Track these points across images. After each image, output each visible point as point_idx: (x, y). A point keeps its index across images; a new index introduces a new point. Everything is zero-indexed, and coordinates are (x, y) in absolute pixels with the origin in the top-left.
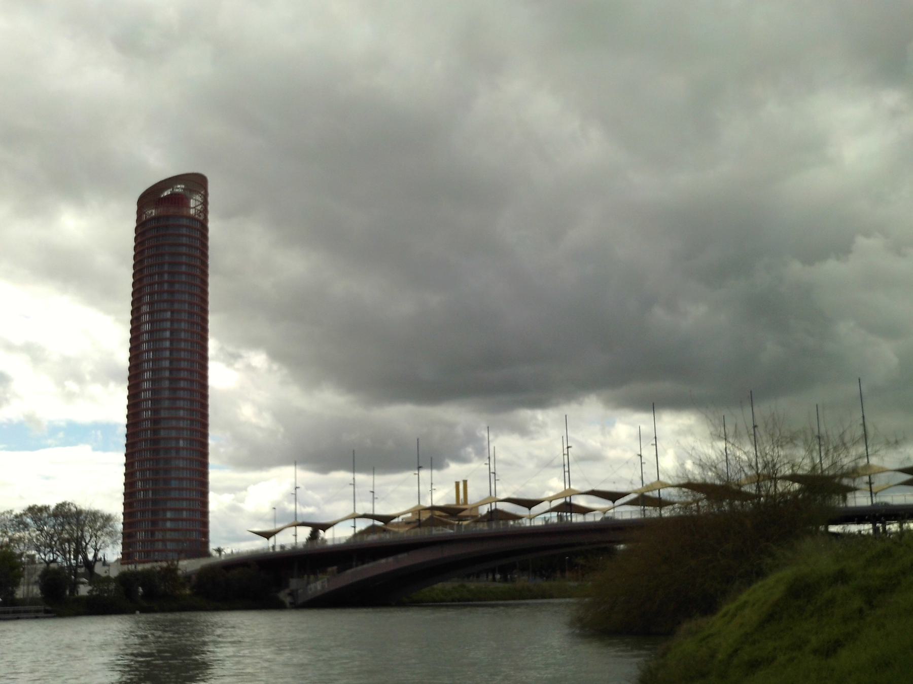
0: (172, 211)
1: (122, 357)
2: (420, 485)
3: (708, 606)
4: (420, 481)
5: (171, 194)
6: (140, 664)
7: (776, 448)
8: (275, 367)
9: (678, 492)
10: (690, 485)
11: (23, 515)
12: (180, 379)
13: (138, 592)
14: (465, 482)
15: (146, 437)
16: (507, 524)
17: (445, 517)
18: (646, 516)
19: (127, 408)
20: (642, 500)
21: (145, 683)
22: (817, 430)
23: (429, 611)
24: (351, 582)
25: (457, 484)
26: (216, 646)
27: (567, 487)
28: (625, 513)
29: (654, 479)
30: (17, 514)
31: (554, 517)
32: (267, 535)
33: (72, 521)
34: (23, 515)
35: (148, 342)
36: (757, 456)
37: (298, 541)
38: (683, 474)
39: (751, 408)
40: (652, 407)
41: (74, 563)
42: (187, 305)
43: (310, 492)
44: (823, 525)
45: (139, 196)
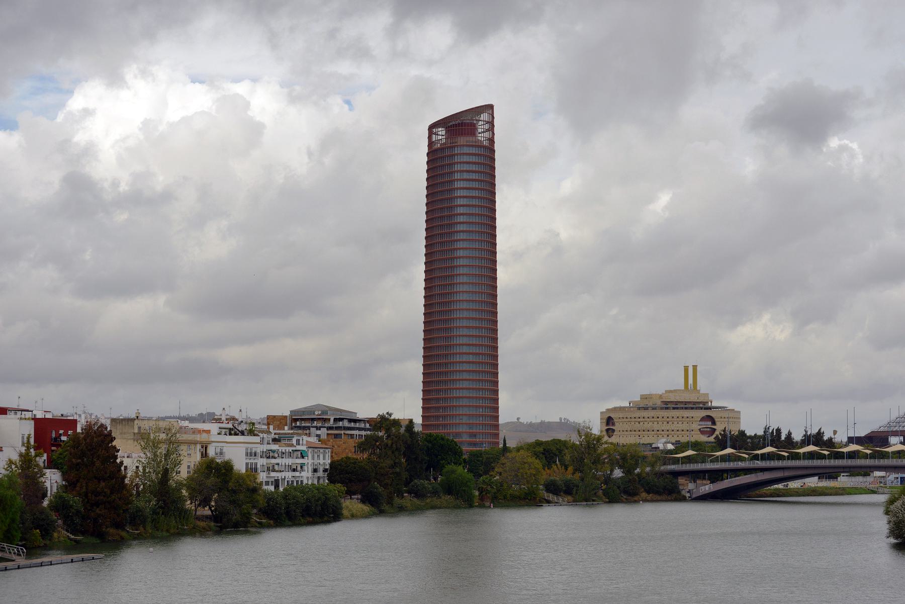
14: (695, 367)
25: (686, 369)
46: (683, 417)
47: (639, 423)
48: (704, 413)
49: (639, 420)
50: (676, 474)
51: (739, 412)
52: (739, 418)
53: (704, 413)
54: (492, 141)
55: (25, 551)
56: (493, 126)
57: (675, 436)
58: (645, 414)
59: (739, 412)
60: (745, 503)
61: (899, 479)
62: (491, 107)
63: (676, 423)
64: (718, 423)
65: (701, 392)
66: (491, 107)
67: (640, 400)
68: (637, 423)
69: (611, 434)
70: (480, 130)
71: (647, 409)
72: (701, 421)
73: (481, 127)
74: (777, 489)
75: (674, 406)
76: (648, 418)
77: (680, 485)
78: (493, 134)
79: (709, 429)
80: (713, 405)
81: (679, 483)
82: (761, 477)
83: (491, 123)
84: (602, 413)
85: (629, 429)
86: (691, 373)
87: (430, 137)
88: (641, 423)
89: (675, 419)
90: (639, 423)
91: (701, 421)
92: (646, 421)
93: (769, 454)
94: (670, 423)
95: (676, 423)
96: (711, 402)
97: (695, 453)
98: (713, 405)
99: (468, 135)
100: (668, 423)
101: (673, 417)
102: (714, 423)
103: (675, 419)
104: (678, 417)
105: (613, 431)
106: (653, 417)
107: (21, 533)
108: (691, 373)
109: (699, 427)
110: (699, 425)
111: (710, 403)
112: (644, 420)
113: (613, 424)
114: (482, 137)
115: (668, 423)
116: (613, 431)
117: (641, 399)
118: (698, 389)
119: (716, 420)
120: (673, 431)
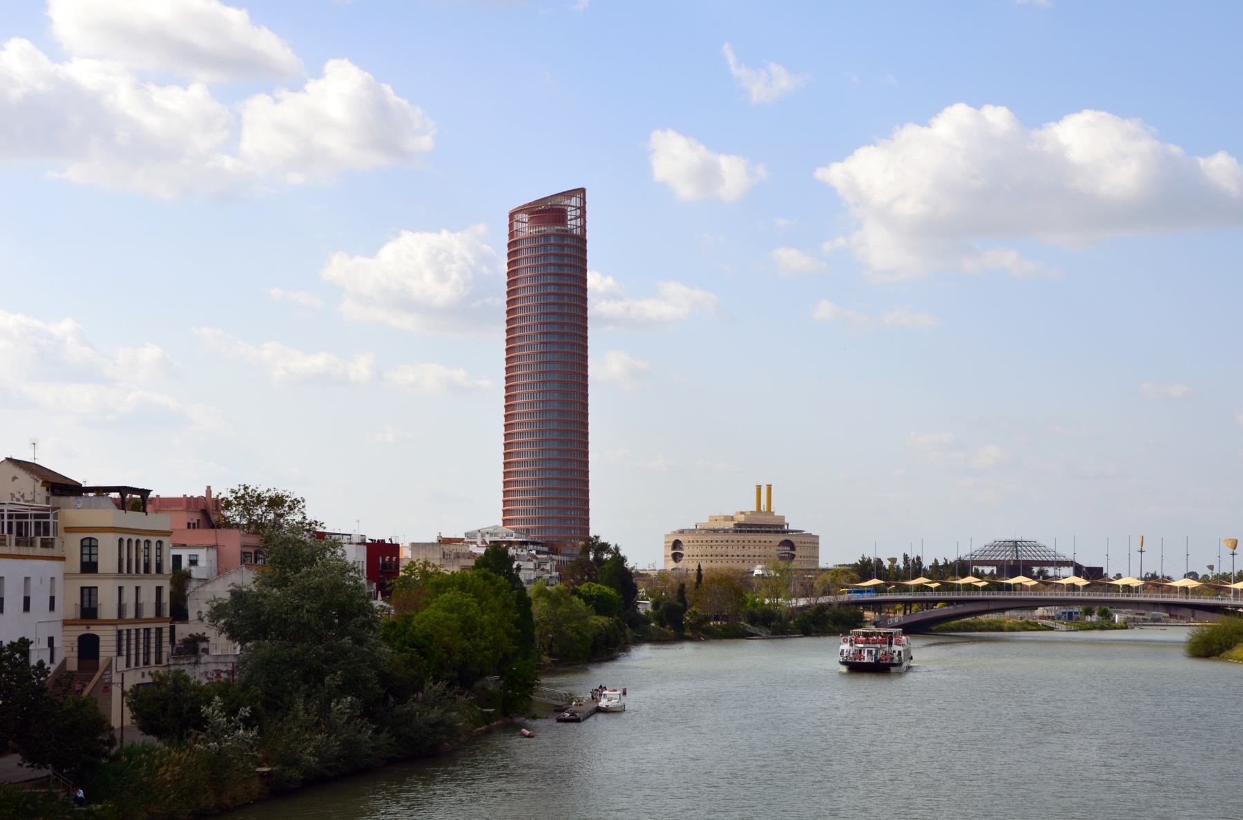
1: (457, 537)
3: (543, 546)
5: (133, 494)
6: (1086, 606)
9: (406, 558)
11: (1200, 577)
14: (769, 487)
16: (1085, 618)
17: (930, 583)
19: (965, 577)
22: (154, 599)
23: (854, 599)
24: (856, 599)
25: (759, 488)
26: (1173, 613)
28: (579, 666)
31: (440, 613)
33: (300, 704)
34: (1200, 577)
35: (266, 506)
38: (354, 563)
39: (124, 724)
42: (552, 238)
44: (197, 645)
46: (760, 542)
47: (711, 547)
48: (782, 538)
49: (711, 544)
50: (858, 603)
51: (817, 537)
52: (818, 543)
53: (782, 538)
54: (583, 227)
55: (259, 769)
56: (585, 212)
57: (724, 562)
58: (716, 537)
59: (817, 537)
60: (946, 643)
61: (1067, 615)
62: (583, 190)
63: (752, 547)
64: (797, 549)
65: (776, 514)
66: (583, 190)
67: (708, 521)
68: (709, 547)
69: (678, 559)
70: (569, 217)
71: (728, 532)
72: (779, 545)
73: (572, 213)
74: (968, 623)
75: (749, 529)
76: (722, 541)
77: (867, 621)
78: (585, 221)
79: (787, 555)
80: (790, 528)
81: (865, 616)
82: (950, 610)
83: (583, 209)
84: (667, 536)
85: (700, 554)
86: (764, 492)
87: (511, 226)
88: (714, 548)
89: (752, 543)
90: (711, 547)
91: (779, 545)
92: (719, 545)
93: (970, 584)
94: (746, 548)
95: (752, 547)
96: (788, 525)
97: (883, 582)
98: (789, 528)
99: (559, 222)
100: (744, 547)
101: (749, 542)
102: (793, 548)
103: (752, 543)
104: (755, 542)
105: (682, 555)
106: (727, 541)
107: (205, 720)
108: (764, 492)
109: (778, 552)
110: (778, 550)
111: (786, 527)
112: (717, 544)
113: (681, 549)
114: (572, 224)
115: (744, 547)
116: (682, 555)
117: (710, 520)
118: (772, 510)
119: (796, 545)
120: (749, 556)
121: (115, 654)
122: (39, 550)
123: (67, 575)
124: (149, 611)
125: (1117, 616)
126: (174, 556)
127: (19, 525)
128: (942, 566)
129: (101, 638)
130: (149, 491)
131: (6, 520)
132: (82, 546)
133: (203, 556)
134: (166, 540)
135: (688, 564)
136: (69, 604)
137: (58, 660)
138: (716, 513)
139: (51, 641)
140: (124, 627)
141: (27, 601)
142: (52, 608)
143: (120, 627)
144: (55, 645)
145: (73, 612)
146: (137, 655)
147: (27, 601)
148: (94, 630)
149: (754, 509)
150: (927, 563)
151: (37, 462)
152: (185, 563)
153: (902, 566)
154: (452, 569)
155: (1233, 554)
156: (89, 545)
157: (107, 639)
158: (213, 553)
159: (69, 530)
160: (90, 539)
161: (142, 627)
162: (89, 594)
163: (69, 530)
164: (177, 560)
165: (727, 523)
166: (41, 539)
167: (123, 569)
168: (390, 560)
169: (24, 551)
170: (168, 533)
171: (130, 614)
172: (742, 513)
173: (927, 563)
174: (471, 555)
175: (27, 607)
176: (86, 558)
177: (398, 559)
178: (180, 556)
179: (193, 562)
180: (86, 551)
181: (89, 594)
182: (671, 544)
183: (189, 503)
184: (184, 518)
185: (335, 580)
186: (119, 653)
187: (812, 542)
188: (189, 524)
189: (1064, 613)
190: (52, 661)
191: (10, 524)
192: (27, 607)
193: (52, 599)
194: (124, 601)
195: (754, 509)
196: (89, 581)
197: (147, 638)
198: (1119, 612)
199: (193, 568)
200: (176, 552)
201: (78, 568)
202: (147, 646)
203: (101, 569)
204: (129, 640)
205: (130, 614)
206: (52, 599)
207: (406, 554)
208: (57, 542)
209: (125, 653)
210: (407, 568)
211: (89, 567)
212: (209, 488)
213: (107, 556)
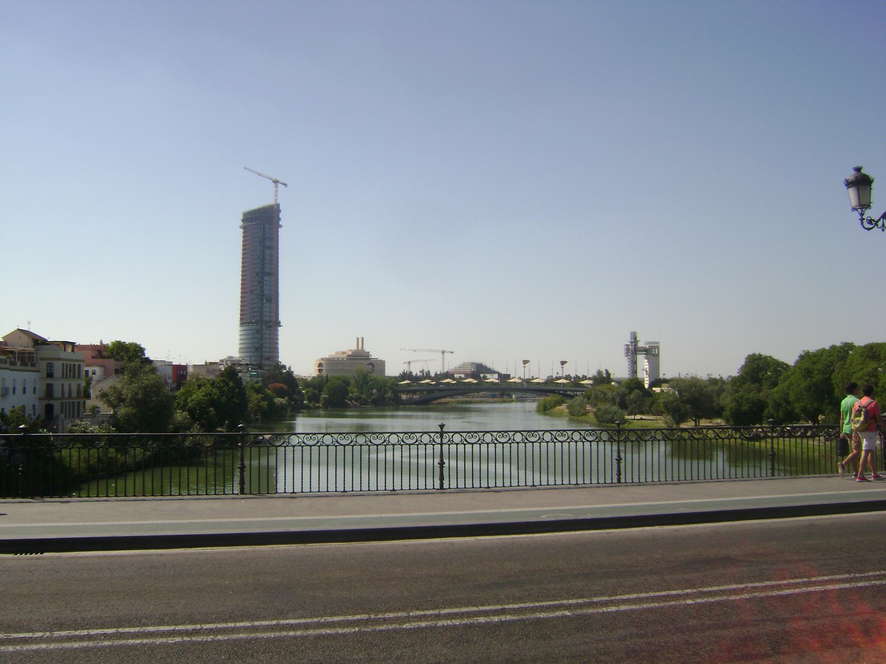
0: (503, 380)
2: (568, 452)
4: (504, 459)
7: (817, 458)
8: (348, 380)
10: (700, 385)
12: (778, 448)
13: (306, 403)
14: (363, 339)
15: (695, 463)
18: (196, 468)
20: (645, 427)
21: (117, 341)
25: (358, 339)
27: (360, 348)
29: (253, 449)
30: (315, 377)
32: (361, 431)
36: (805, 560)
37: (710, 462)
40: (471, 460)
41: (133, 410)
43: (74, 427)
45: (871, 342)
53: (368, 362)
64: (376, 367)
86: (361, 341)
108: (361, 341)
117: (6, 388)
121: (60, 412)
122: (30, 368)
123: (41, 378)
124: (74, 394)
125: (513, 396)
126: (86, 371)
127: (22, 357)
128: (439, 374)
129: (55, 406)
130: (75, 343)
131: (17, 355)
132: (47, 367)
133: (98, 370)
134: (82, 364)
135: (324, 373)
136: (41, 390)
137: (37, 413)
138: (338, 350)
139: (34, 406)
140: (64, 401)
141: (24, 389)
142: (35, 392)
143: (63, 401)
144: (36, 408)
145: (43, 394)
146: (69, 413)
147: (24, 389)
148: (52, 402)
149: (356, 349)
150: (432, 374)
151: (30, 330)
152: (90, 374)
153: (605, 376)
154: (212, 377)
155: (562, 368)
156: (50, 366)
157: (57, 405)
158: (102, 369)
159: (42, 359)
160: (51, 363)
161: (71, 401)
162: (50, 387)
163: (42, 359)
164: (87, 372)
165: (343, 355)
166: (119, 370)
167: (64, 376)
168: (183, 372)
169: (24, 368)
170: (83, 361)
171: (66, 395)
172: (350, 350)
173: (432, 374)
174: (220, 370)
175: (24, 392)
176: (49, 371)
177: (187, 372)
178: (88, 371)
179: (94, 373)
180: (49, 368)
181: (50, 387)
182: (317, 365)
183: (92, 347)
184: (91, 353)
185: (149, 567)
186: (62, 412)
187: (382, 364)
188: (92, 357)
189: (491, 395)
190: (34, 415)
191: (18, 356)
192: (24, 392)
193: (35, 388)
194: (65, 390)
195: (356, 349)
196: (50, 381)
197: (74, 406)
198: (514, 394)
199: (94, 376)
200: (86, 369)
201: (45, 375)
202: (74, 409)
203: (54, 376)
204: (69, 406)
205: (66, 395)
206: (35, 388)
207: (190, 370)
208: (37, 365)
209: (64, 411)
210: (191, 376)
211: (50, 375)
212: (101, 340)
213: (58, 371)
